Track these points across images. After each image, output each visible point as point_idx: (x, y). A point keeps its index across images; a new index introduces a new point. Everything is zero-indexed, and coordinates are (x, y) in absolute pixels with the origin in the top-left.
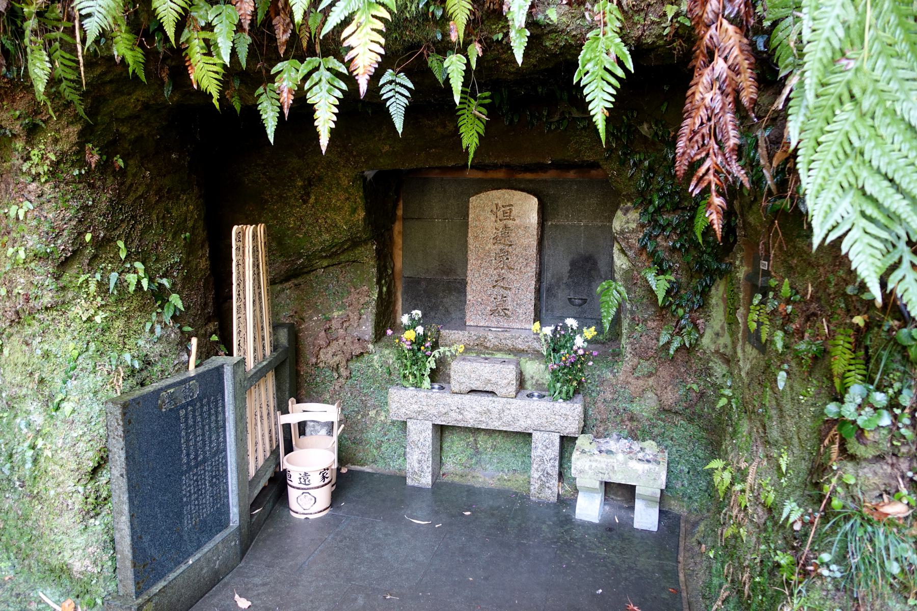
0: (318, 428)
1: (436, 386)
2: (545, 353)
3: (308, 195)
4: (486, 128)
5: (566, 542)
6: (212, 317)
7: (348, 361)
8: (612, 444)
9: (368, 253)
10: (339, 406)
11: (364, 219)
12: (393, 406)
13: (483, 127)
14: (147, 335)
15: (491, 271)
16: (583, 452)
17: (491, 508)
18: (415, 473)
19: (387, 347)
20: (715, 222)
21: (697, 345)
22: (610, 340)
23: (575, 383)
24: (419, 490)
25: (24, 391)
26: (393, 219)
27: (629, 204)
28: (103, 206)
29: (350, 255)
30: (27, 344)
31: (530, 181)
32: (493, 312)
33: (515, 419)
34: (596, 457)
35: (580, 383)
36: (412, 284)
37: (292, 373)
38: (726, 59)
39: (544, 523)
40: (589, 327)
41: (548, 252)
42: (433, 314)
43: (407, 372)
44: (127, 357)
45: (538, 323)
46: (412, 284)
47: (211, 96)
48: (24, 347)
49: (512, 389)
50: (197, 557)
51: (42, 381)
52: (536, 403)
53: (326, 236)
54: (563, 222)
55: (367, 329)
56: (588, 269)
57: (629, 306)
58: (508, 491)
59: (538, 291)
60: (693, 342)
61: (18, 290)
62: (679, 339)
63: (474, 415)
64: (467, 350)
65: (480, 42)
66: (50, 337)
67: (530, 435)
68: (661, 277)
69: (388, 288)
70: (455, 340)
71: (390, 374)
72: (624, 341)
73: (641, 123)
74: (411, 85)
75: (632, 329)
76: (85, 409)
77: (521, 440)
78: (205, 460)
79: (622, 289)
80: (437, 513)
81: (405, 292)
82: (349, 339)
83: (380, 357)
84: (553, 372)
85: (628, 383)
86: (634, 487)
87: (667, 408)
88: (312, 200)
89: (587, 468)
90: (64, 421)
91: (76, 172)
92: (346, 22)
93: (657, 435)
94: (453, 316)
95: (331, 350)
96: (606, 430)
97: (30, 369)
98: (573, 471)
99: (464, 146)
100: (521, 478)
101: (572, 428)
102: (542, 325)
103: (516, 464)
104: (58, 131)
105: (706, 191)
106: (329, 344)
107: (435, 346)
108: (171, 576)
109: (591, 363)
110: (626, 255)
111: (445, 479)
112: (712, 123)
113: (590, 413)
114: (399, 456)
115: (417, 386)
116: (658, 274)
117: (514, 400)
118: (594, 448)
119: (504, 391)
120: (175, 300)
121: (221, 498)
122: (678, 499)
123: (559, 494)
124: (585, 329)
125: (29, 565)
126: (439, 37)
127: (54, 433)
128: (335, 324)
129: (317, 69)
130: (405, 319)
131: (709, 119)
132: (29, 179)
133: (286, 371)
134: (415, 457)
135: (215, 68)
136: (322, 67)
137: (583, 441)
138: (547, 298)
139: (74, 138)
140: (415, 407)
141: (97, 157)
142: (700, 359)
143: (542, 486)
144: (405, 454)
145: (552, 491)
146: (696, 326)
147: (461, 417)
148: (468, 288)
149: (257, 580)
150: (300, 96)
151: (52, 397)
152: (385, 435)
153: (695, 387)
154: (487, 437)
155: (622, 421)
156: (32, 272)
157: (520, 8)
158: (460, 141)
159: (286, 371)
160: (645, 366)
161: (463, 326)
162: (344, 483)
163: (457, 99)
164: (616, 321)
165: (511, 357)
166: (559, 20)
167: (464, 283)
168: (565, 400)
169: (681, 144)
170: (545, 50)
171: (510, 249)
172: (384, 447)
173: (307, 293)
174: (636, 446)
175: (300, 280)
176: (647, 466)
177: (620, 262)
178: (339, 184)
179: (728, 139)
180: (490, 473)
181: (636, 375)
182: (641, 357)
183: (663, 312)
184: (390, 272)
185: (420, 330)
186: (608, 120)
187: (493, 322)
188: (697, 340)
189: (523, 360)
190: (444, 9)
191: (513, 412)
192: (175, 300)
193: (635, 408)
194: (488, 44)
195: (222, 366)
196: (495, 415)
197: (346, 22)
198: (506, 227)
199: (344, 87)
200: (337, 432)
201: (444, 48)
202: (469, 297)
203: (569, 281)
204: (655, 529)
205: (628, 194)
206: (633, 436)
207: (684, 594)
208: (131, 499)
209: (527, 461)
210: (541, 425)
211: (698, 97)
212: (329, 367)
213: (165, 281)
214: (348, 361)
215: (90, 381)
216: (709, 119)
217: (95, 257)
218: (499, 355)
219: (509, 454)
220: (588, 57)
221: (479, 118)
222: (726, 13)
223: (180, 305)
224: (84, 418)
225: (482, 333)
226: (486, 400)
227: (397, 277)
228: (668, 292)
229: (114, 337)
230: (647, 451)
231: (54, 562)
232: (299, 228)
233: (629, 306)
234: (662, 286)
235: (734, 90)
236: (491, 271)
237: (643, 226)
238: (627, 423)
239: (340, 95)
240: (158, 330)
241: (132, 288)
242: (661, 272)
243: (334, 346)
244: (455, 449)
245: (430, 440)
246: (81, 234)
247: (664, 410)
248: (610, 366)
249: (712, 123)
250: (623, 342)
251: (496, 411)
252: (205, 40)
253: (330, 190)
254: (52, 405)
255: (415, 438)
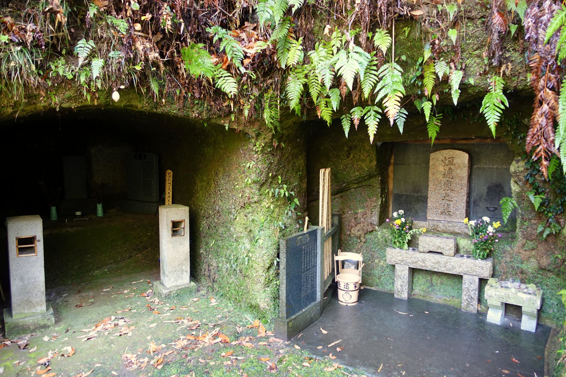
0: (350, 265)
1: (411, 248)
2: (471, 234)
3: (350, 154)
4: (440, 129)
5: (481, 330)
6: (309, 208)
7: (365, 234)
8: (509, 284)
9: (376, 182)
10: (362, 254)
11: (376, 165)
12: (388, 257)
13: (438, 128)
14: (285, 215)
15: (441, 191)
16: (492, 286)
17: (440, 312)
18: (399, 291)
19: (385, 228)
20: (544, 172)
21: (559, 233)
22: (511, 231)
23: (488, 251)
24: (401, 300)
25: (243, 235)
26: (389, 164)
27: (519, 158)
28: (276, 162)
29: (367, 183)
30: (246, 216)
31: (464, 144)
32: (442, 213)
33: (453, 268)
34: (499, 289)
35: (491, 251)
36: (398, 198)
37: (340, 239)
38: (548, 104)
39: (469, 321)
40: (496, 221)
41: (474, 182)
42: (408, 213)
43: (396, 240)
44: (280, 223)
45: (467, 219)
46: (398, 198)
47: (327, 122)
48: (245, 217)
49: (452, 252)
50: (306, 309)
51: (250, 231)
52: (465, 260)
53: (357, 173)
54: (483, 166)
55: (375, 219)
56: (498, 191)
57: (520, 212)
58: (449, 306)
59: (468, 203)
60: (557, 231)
61: (246, 195)
62: (549, 229)
63: (431, 264)
64: (427, 231)
65: (438, 93)
66: (255, 213)
67: (462, 276)
68: (537, 196)
69: (386, 199)
70: (421, 226)
71: (386, 242)
72: (518, 230)
73: (524, 118)
74: (407, 113)
75: (522, 224)
76: (266, 243)
77: (456, 280)
78: (309, 269)
79: (514, 202)
80: (411, 310)
81: (394, 202)
82: (366, 224)
83: (381, 233)
84: (475, 244)
85: (520, 253)
86: (521, 307)
87: (543, 267)
88: (351, 156)
89: (493, 294)
90: (259, 247)
91: (269, 150)
92: (385, 96)
93: (538, 283)
94: (420, 214)
95: (357, 228)
96: (506, 278)
97: (245, 226)
98: (485, 295)
99: (430, 136)
100: (457, 301)
101: (486, 274)
102: (469, 220)
103: (454, 293)
104: (266, 135)
105: (539, 159)
106: (356, 226)
107: (410, 228)
108: (297, 314)
109: (497, 241)
110: (518, 184)
111: (415, 297)
112: (542, 130)
113: (497, 268)
114: (390, 283)
115: (401, 248)
116: (536, 194)
117: (453, 258)
118: (498, 285)
119: (447, 253)
120: (296, 201)
121: (314, 287)
122: (550, 319)
123: (478, 310)
124: (494, 223)
125: (241, 305)
126: (420, 93)
127: (256, 251)
128: (359, 216)
129: (369, 111)
130: (395, 214)
131: (541, 129)
132: (254, 153)
133: (337, 237)
134: (399, 283)
135: (330, 112)
136: (371, 110)
137: (491, 281)
138: (473, 206)
139: (270, 137)
140: (400, 258)
141: (277, 144)
142: (563, 241)
143: (469, 304)
144: (393, 283)
145: (474, 307)
146: (558, 223)
147: (424, 264)
148: (429, 200)
149: (328, 325)
150: (362, 120)
151: (254, 237)
152: (383, 272)
153: (560, 256)
154: (437, 278)
155: (516, 273)
156: (252, 188)
157: (456, 82)
158: (427, 134)
159: (337, 237)
160: (530, 244)
161: (425, 219)
162: (363, 293)
163: (427, 119)
164: (512, 220)
165: (452, 236)
166: (475, 82)
167: (426, 198)
168: (482, 259)
169: (528, 139)
170: (469, 94)
171: (452, 180)
172: (382, 278)
173: (346, 201)
174: (523, 286)
175: (343, 194)
176: (529, 296)
177: (515, 188)
178: (364, 149)
179: (550, 137)
180: (440, 295)
181: (524, 249)
182: (527, 239)
183: (540, 214)
184: (386, 191)
185: (403, 220)
186: (496, 127)
187: (442, 218)
188: (560, 230)
189: (458, 238)
190: (422, 82)
191: (452, 264)
192: (296, 201)
193: (524, 267)
194: (441, 94)
195: (317, 230)
196: (442, 265)
197: (385, 96)
198: (450, 169)
199: (380, 117)
200: (361, 266)
201: (421, 97)
202: (429, 205)
203: (485, 197)
204: (534, 331)
205: (518, 153)
206: (523, 281)
207: (546, 360)
208: (287, 278)
209: (460, 292)
210: (468, 271)
211: (536, 120)
212: (356, 237)
213: (292, 193)
214: (365, 234)
215: (268, 232)
216: (541, 129)
217: (271, 182)
218: (445, 235)
219: (450, 288)
220: (487, 101)
221: (437, 125)
222: (548, 85)
223: (298, 203)
224: (266, 246)
225: (435, 223)
226: (437, 256)
227: (390, 193)
228: (542, 204)
229: (275, 215)
230: (530, 289)
231: (253, 303)
232: (345, 169)
233: (520, 212)
234: (538, 201)
235: (552, 117)
236: (441, 191)
237: (527, 169)
238: (519, 274)
239: (378, 120)
240: (290, 213)
241: (282, 195)
242: (537, 193)
243: (359, 227)
244: (420, 282)
245: (407, 275)
246: (268, 173)
247: (541, 269)
248: (510, 244)
249: (542, 130)
250: (517, 231)
251: (443, 262)
252: (326, 101)
253: (360, 152)
254: (253, 240)
255: (400, 274)
